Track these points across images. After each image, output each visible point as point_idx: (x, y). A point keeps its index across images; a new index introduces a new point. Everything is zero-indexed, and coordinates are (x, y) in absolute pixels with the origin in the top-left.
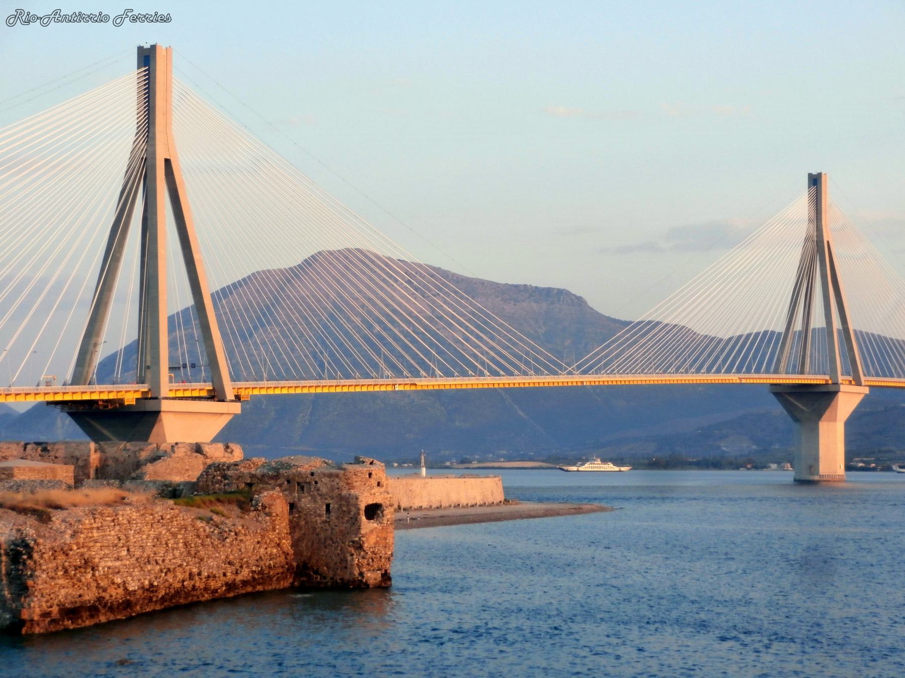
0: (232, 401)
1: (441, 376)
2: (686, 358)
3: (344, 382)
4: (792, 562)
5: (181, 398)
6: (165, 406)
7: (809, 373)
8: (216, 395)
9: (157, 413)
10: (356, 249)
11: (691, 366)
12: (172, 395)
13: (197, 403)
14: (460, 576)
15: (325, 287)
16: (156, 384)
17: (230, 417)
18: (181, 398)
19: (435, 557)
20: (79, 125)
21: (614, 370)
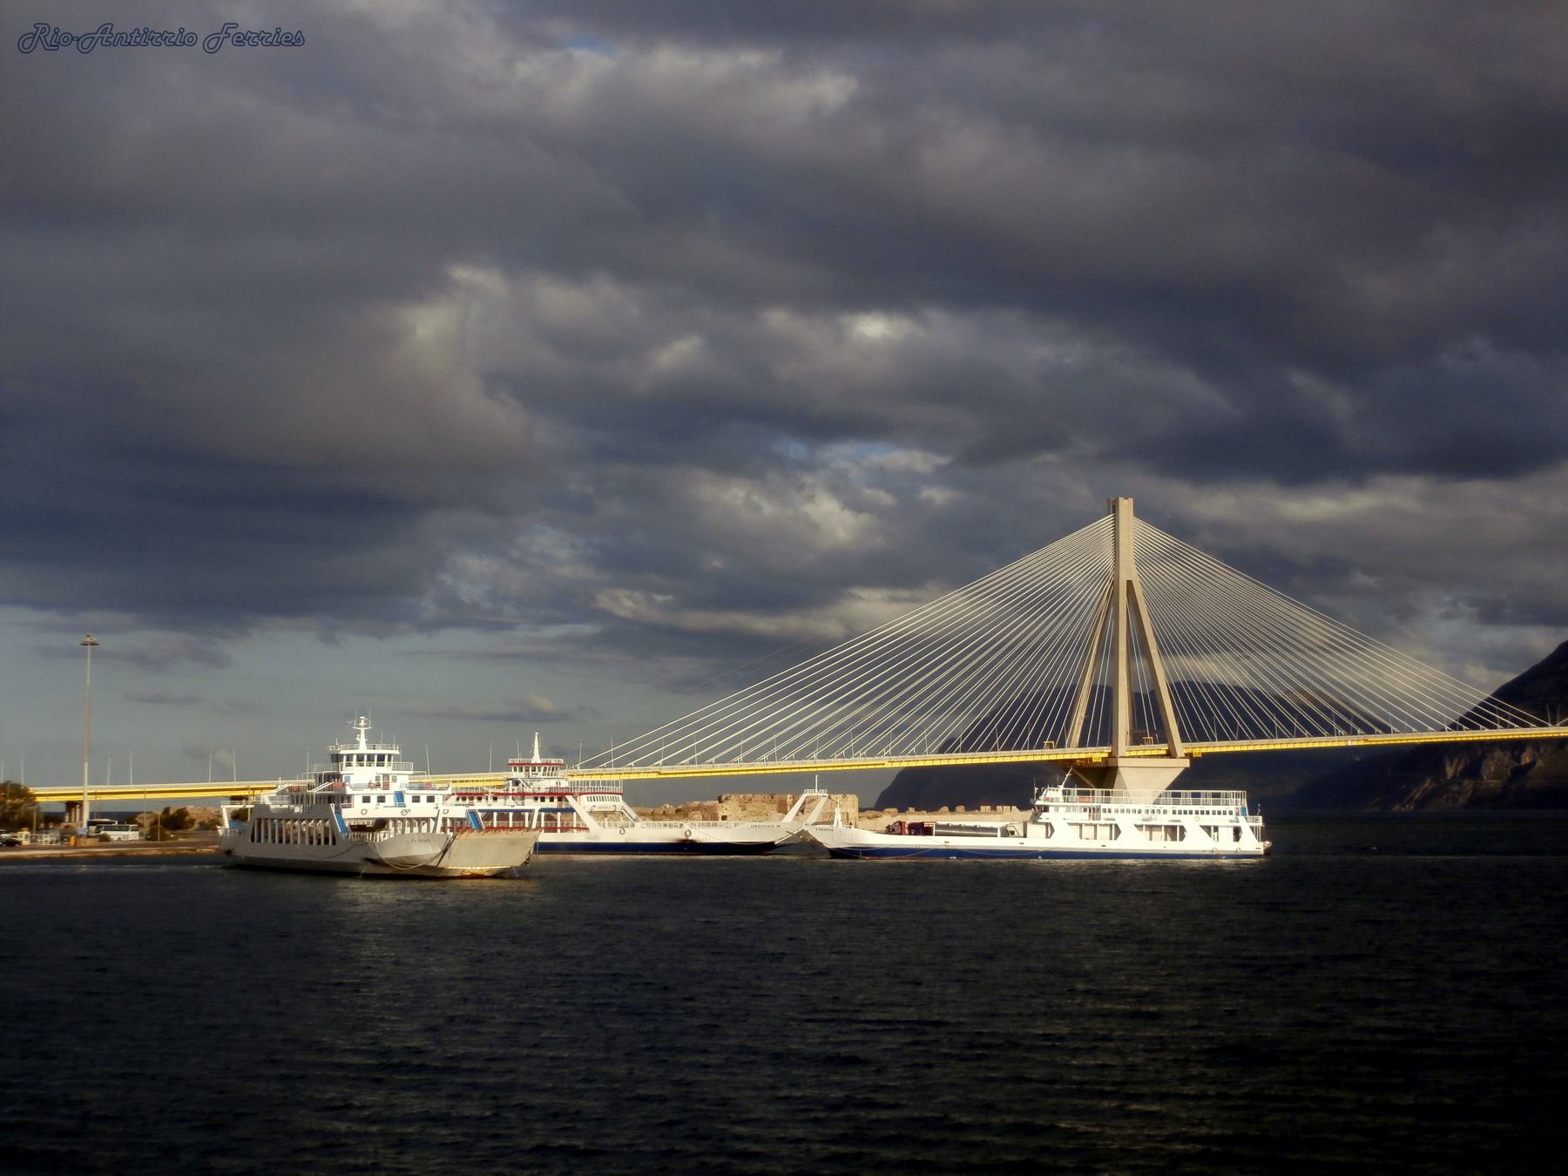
0: (1182, 758)
1: (1449, 730)
2: (994, 733)
3: (1278, 740)
4: (527, 998)
5: (1139, 757)
6: (1121, 762)
7: (374, 755)
8: (1170, 754)
9: (1116, 768)
10: (1219, 685)
11: (931, 738)
12: (1127, 754)
13: (1136, 759)
14: (744, 1013)
15: (985, 693)
16: (1116, 748)
17: (1182, 769)
18: (1139, 757)
19: (702, 983)
20: (1017, 637)
21: (992, 739)
